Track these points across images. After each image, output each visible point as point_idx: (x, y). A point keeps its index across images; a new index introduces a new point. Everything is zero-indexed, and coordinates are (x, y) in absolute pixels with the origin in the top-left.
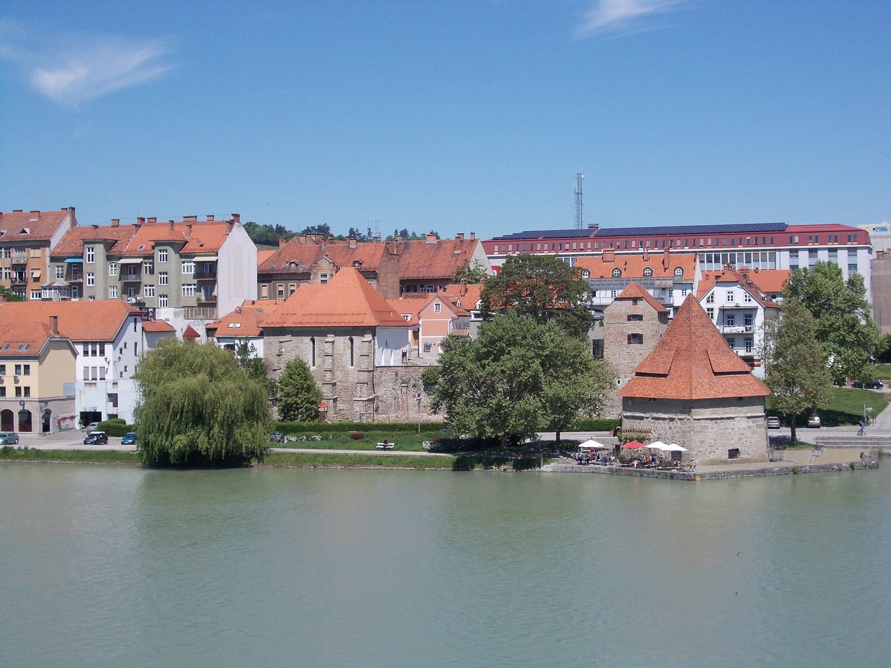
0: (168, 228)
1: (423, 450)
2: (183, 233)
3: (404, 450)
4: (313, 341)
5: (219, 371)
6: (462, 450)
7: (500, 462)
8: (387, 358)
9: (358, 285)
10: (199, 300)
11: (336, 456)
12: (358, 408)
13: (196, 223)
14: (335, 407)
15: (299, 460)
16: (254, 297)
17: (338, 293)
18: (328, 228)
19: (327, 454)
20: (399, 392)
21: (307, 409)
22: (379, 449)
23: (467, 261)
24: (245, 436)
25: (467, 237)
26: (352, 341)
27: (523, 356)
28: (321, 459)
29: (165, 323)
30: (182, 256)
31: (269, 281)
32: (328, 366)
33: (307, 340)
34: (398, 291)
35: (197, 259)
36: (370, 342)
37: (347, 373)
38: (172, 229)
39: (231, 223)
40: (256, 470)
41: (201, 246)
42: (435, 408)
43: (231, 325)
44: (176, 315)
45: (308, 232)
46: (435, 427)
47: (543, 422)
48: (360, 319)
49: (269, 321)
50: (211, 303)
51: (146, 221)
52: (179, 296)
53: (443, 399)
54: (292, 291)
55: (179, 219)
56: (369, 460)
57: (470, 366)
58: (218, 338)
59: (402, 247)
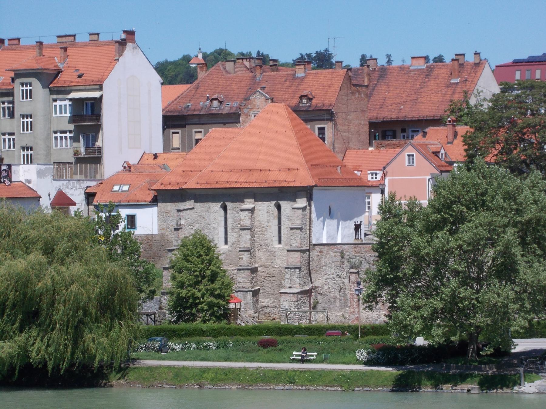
0: (35, 52)
1: (358, 362)
2: (56, 59)
3: (330, 362)
4: (225, 208)
5: (61, 248)
6: (413, 362)
7: (462, 378)
8: (333, 232)
9: (289, 128)
10: (76, 153)
11: (231, 370)
12: (287, 303)
13: (74, 44)
14: (256, 302)
15: (179, 377)
16: (158, 148)
17: (265, 141)
18: (330, 56)
19: (218, 369)
20: (346, 281)
21: (211, 305)
22: (294, 361)
23: (466, 94)
24: (98, 343)
25: (470, 58)
26: (279, 208)
27: (490, 224)
28: (210, 376)
29: (25, 185)
30: (53, 92)
31: (182, 126)
32: (245, 243)
33: (216, 207)
34: (365, 137)
35: (73, 95)
36: (304, 209)
37: (272, 254)
38: (41, 54)
39: (122, 43)
40: (119, 389)
41: (80, 76)
42: (371, 299)
43: (116, 188)
44: (40, 174)
45: (302, 61)
46: (375, 330)
47: (519, 322)
48: (290, 176)
49: (166, 181)
50: (93, 158)
51: (6, 42)
52: (49, 149)
53: (381, 289)
54: (198, 141)
55: (50, 40)
56: (277, 377)
57: (417, 239)
58: (96, 207)
59: (376, 75)
